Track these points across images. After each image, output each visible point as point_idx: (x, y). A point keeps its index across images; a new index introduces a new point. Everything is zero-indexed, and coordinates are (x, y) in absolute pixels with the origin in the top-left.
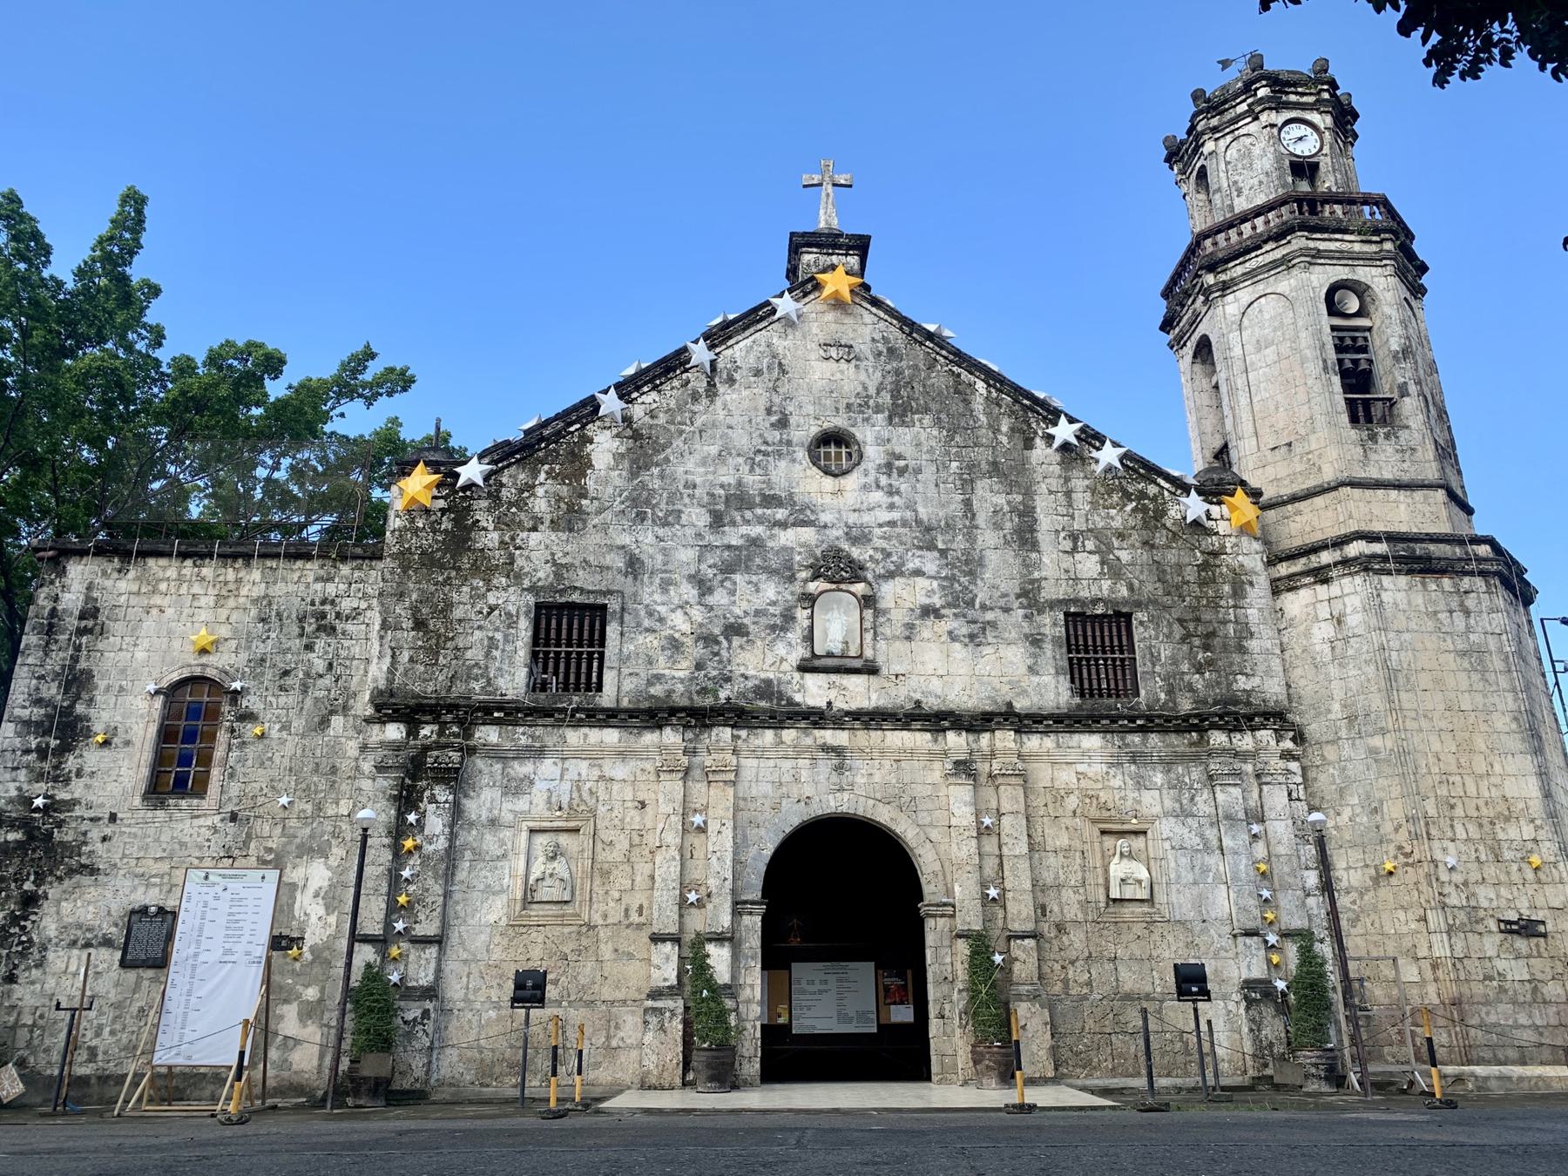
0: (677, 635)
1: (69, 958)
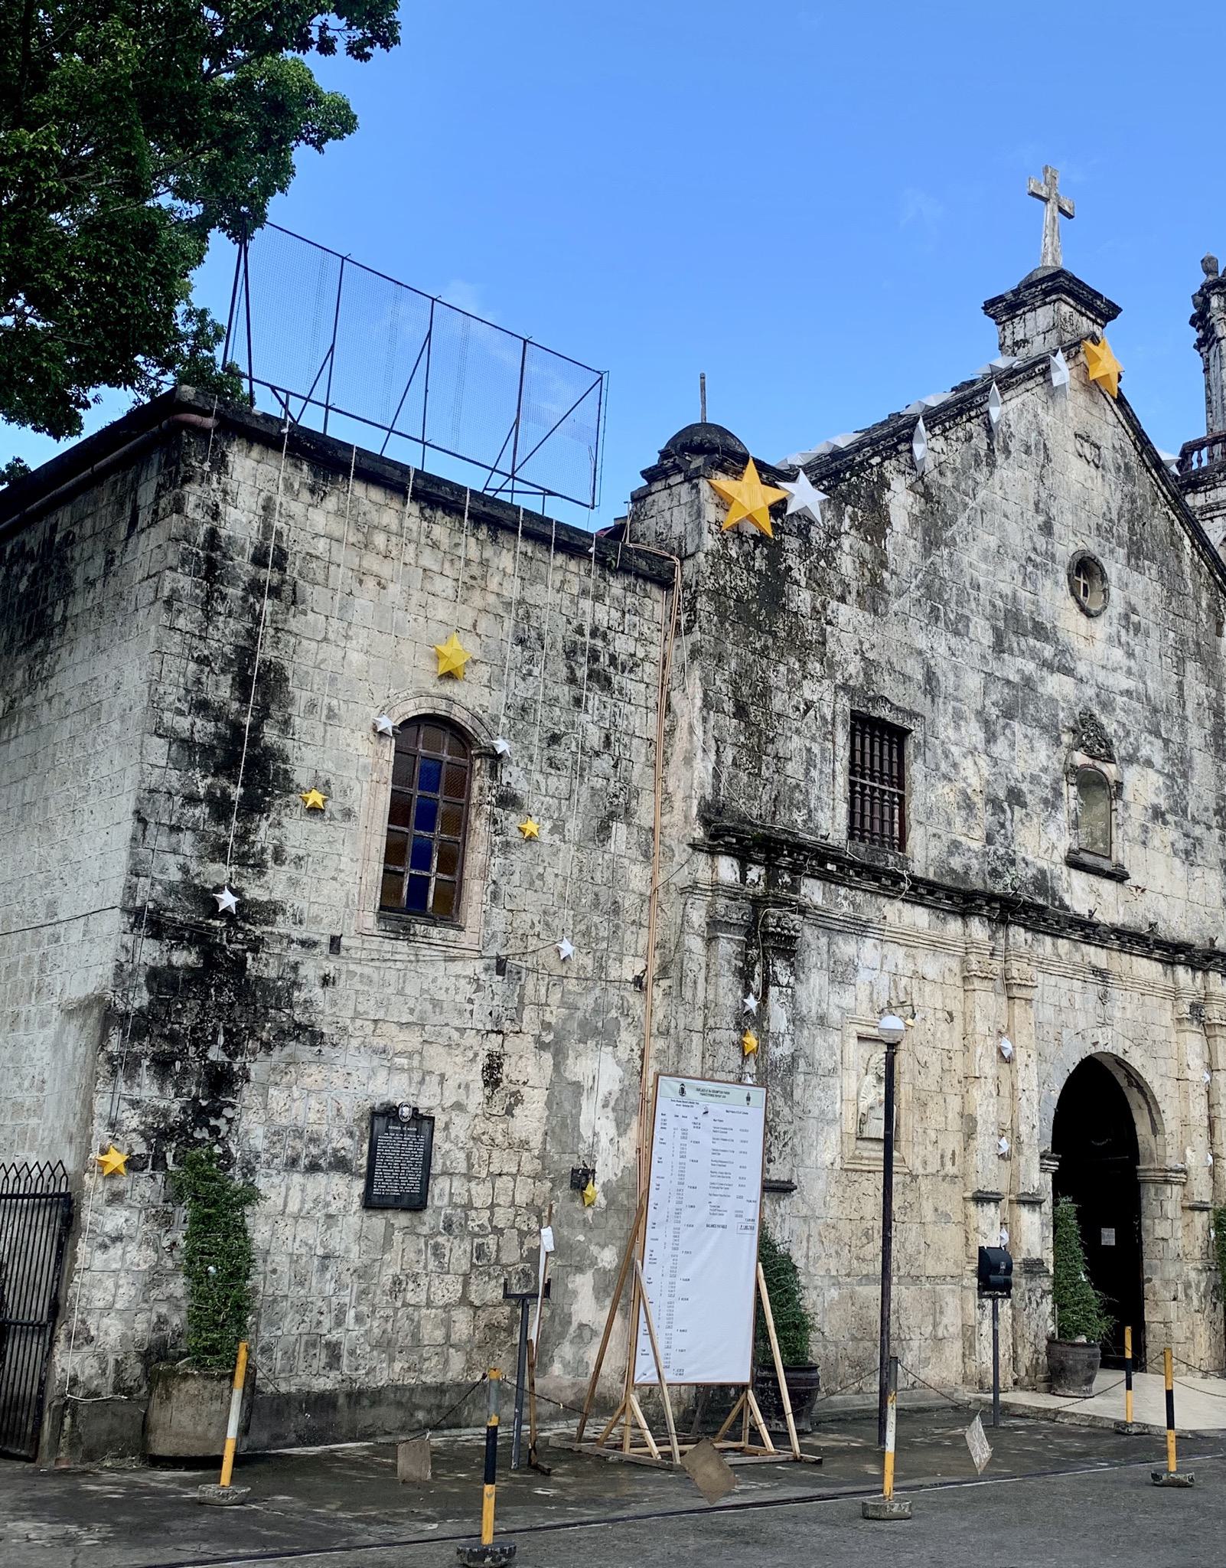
0: (969, 791)
1: (288, 1189)
